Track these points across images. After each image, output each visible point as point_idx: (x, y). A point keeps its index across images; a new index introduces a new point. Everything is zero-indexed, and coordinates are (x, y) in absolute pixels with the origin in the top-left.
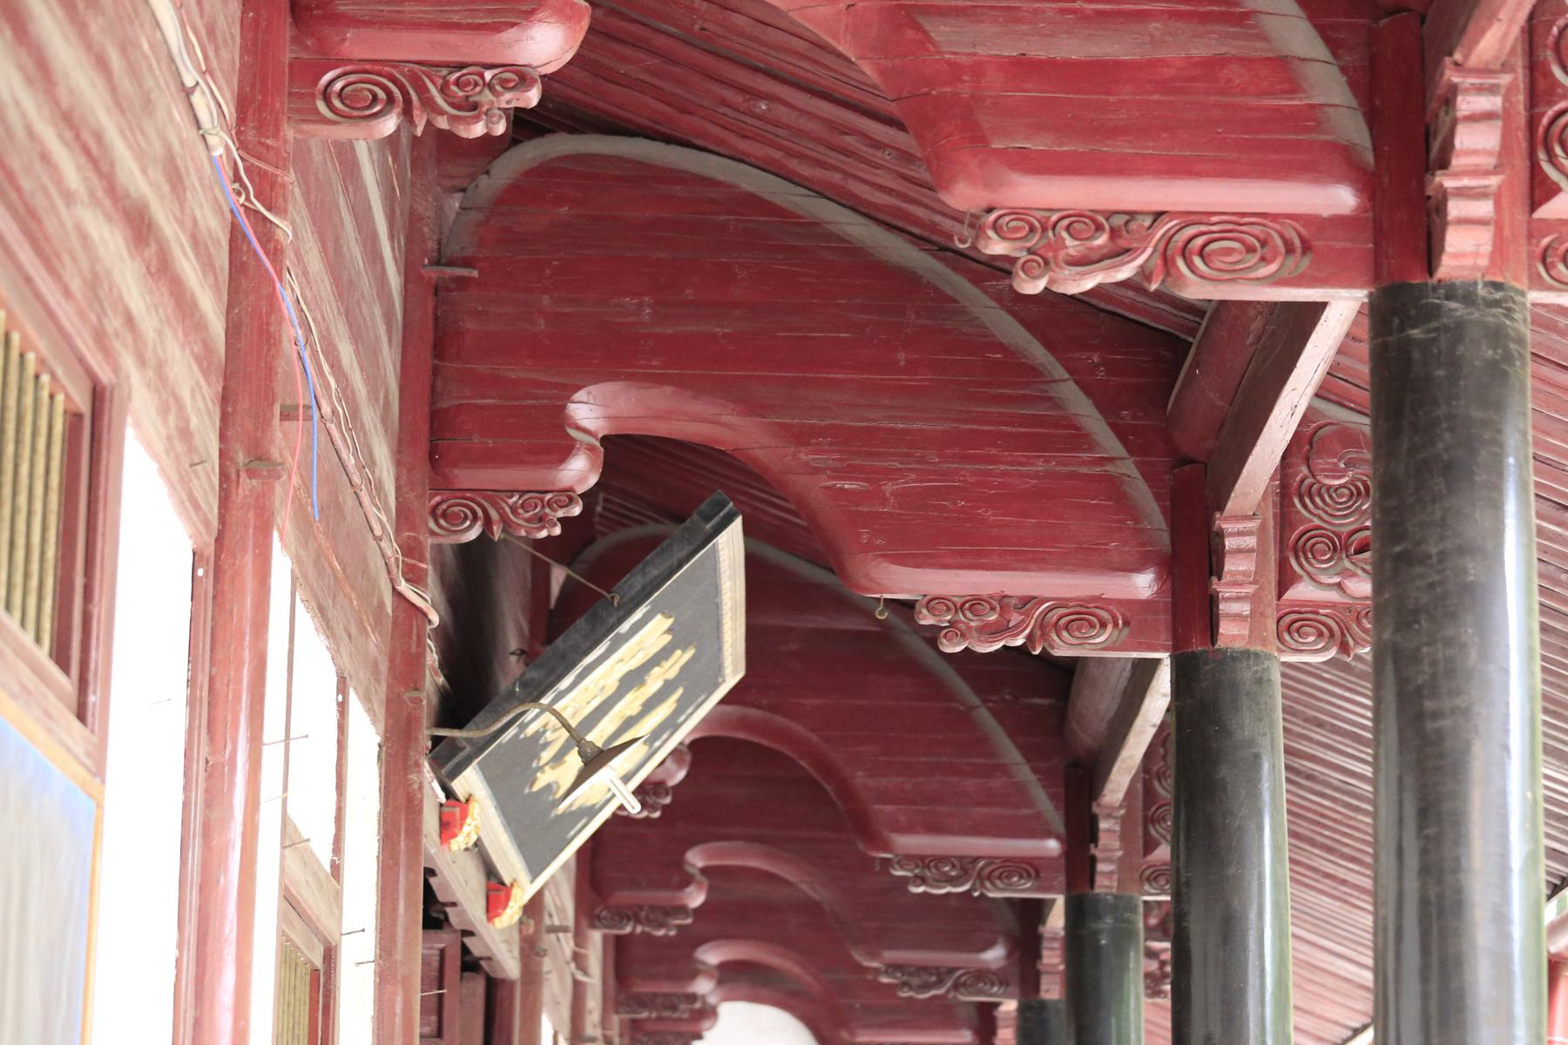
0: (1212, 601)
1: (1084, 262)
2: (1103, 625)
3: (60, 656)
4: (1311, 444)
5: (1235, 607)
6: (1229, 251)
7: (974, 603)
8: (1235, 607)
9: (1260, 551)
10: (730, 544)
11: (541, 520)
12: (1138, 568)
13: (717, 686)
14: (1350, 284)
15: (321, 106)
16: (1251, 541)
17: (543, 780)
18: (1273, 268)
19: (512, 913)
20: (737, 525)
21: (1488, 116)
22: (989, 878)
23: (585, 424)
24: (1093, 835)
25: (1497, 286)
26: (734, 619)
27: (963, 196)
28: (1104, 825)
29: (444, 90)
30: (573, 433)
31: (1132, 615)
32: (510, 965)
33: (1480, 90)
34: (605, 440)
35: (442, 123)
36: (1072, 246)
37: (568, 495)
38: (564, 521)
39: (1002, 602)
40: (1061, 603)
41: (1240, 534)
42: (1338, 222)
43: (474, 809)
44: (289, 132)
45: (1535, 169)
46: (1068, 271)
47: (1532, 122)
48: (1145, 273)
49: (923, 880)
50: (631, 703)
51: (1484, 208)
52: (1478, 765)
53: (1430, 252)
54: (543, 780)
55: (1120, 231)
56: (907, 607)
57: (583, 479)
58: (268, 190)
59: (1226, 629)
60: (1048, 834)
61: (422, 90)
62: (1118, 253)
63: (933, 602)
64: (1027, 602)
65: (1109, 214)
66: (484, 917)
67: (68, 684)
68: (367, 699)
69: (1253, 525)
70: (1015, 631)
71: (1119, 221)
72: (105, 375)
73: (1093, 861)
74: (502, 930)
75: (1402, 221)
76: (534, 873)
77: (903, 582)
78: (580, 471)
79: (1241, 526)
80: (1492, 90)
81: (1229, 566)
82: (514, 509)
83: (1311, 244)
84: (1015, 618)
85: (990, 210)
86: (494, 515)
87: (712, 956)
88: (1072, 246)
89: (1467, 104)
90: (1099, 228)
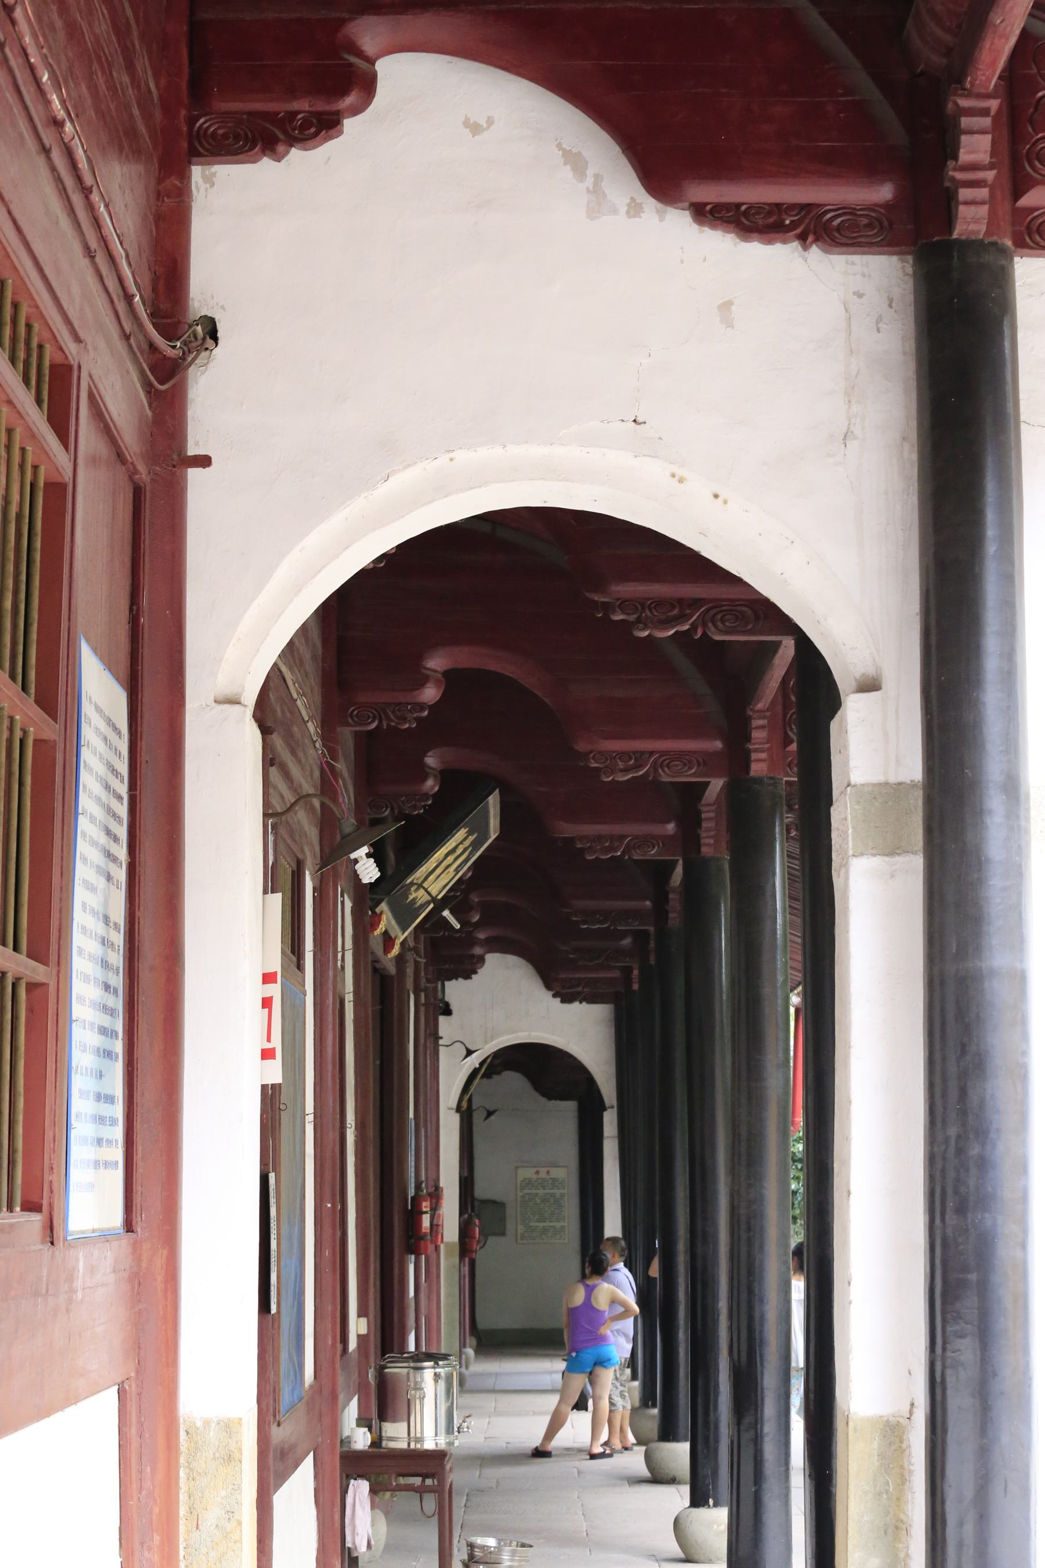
0: (698, 838)
1: (626, 770)
2: (654, 847)
3: (293, 952)
4: (1036, 109)
5: (707, 841)
6: (677, 766)
7: (599, 838)
8: (707, 841)
9: (992, 201)
10: (493, 802)
11: (415, 807)
12: (669, 822)
13: (487, 840)
14: (721, 777)
15: (350, 720)
16: (712, 815)
17: (411, 897)
18: (693, 771)
19: (396, 950)
20: (497, 790)
21: (763, 727)
22: (634, 848)
23: (432, 765)
24: (666, 900)
25: (772, 778)
26: (495, 807)
27: (581, 746)
28: (671, 896)
29: (393, 712)
30: (428, 770)
31: (667, 841)
32: (392, 970)
33: (760, 718)
34: (441, 772)
35: (393, 724)
36: (621, 765)
37: (426, 796)
38: (424, 807)
39: (611, 838)
40: (636, 837)
41: (708, 811)
42: (715, 754)
43: (384, 917)
44: (339, 729)
45: (786, 733)
46: (620, 774)
47: (785, 716)
48: (647, 774)
49: (585, 922)
50: (450, 859)
51: (763, 756)
52: (766, 956)
53: (747, 768)
54: (411, 897)
55: (640, 757)
56: (571, 841)
57: (433, 787)
58: (334, 757)
59: (704, 850)
60: (645, 899)
61: (386, 714)
62: (638, 767)
63: (582, 838)
64: (622, 837)
65: (634, 753)
66: (382, 950)
67: (294, 959)
68: (349, 897)
69: (714, 808)
70: (616, 850)
71: (638, 755)
72: (301, 857)
73: (667, 913)
74: (391, 959)
75: (737, 757)
76: (404, 930)
77: (567, 829)
78: (431, 785)
79: (708, 808)
80: (764, 718)
81: (704, 824)
82: (403, 802)
83: (708, 763)
84: (616, 844)
85: (591, 752)
86: (395, 805)
87: (481, 936)
88: (621, 765)
89: (756, 723)
90: (631, 758)
